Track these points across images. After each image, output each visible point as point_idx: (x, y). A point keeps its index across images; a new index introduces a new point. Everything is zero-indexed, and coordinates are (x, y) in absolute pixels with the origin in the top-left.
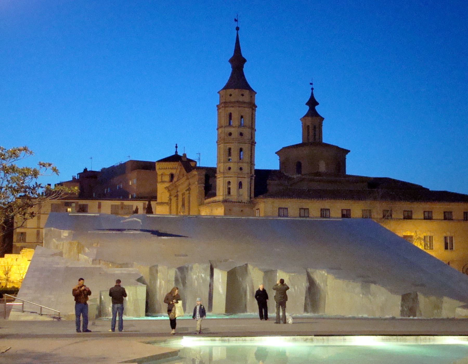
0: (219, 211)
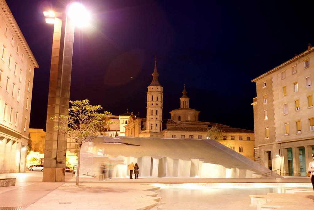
0: (148, 136)
